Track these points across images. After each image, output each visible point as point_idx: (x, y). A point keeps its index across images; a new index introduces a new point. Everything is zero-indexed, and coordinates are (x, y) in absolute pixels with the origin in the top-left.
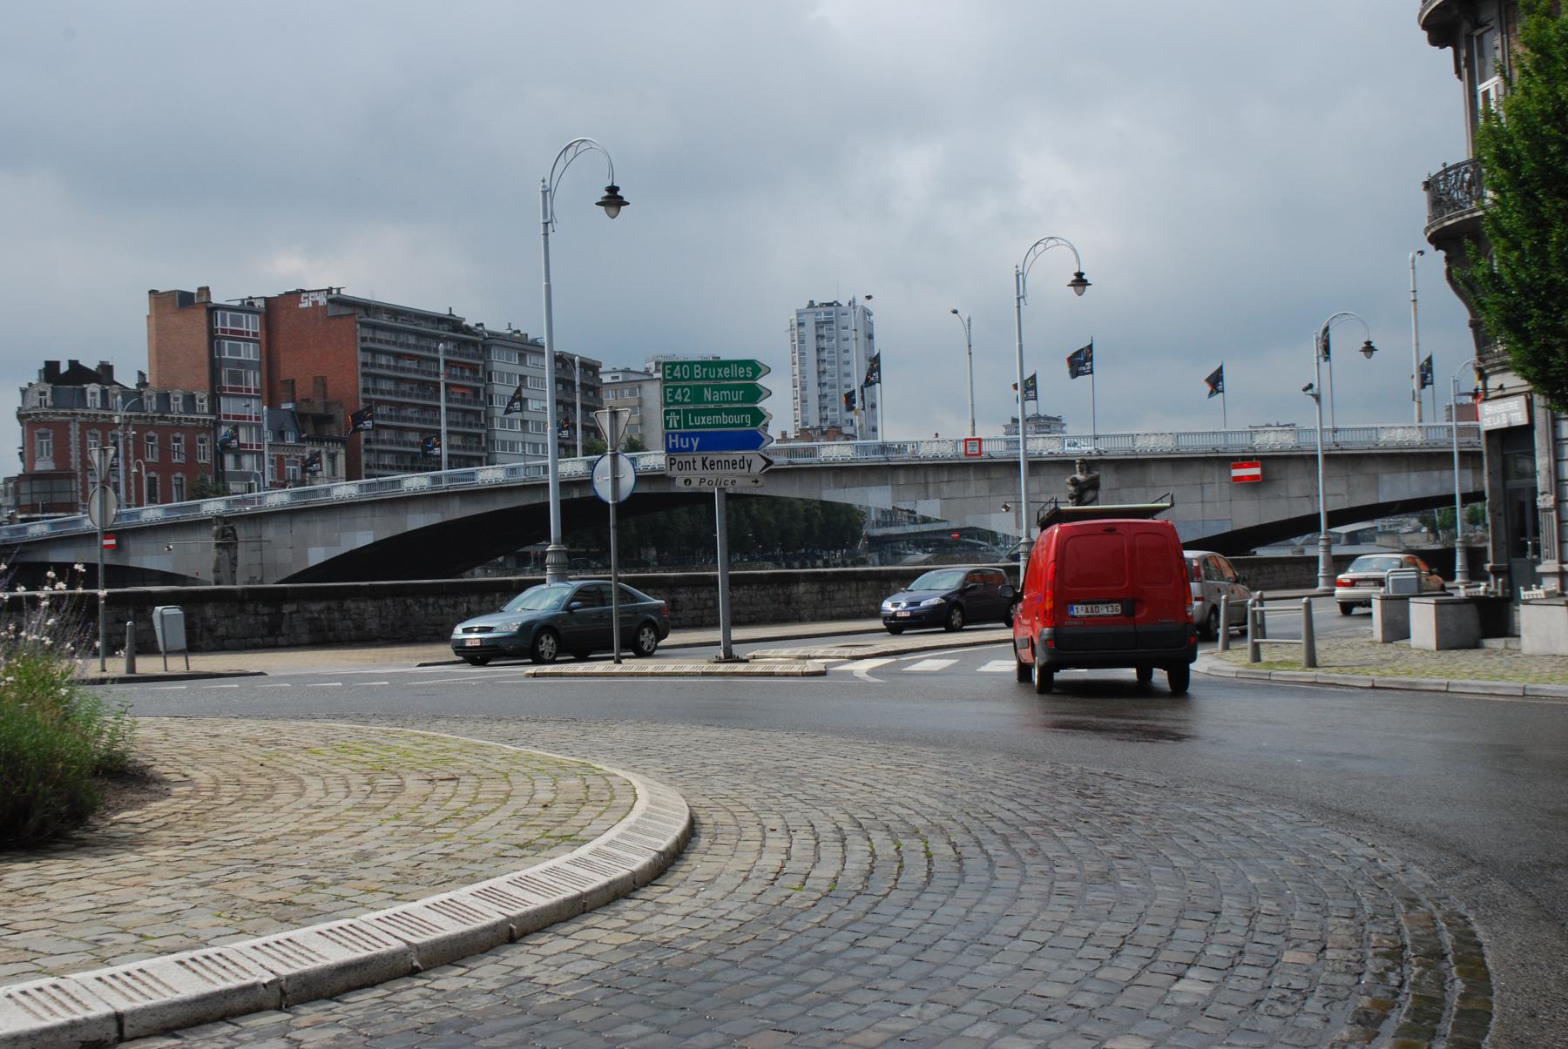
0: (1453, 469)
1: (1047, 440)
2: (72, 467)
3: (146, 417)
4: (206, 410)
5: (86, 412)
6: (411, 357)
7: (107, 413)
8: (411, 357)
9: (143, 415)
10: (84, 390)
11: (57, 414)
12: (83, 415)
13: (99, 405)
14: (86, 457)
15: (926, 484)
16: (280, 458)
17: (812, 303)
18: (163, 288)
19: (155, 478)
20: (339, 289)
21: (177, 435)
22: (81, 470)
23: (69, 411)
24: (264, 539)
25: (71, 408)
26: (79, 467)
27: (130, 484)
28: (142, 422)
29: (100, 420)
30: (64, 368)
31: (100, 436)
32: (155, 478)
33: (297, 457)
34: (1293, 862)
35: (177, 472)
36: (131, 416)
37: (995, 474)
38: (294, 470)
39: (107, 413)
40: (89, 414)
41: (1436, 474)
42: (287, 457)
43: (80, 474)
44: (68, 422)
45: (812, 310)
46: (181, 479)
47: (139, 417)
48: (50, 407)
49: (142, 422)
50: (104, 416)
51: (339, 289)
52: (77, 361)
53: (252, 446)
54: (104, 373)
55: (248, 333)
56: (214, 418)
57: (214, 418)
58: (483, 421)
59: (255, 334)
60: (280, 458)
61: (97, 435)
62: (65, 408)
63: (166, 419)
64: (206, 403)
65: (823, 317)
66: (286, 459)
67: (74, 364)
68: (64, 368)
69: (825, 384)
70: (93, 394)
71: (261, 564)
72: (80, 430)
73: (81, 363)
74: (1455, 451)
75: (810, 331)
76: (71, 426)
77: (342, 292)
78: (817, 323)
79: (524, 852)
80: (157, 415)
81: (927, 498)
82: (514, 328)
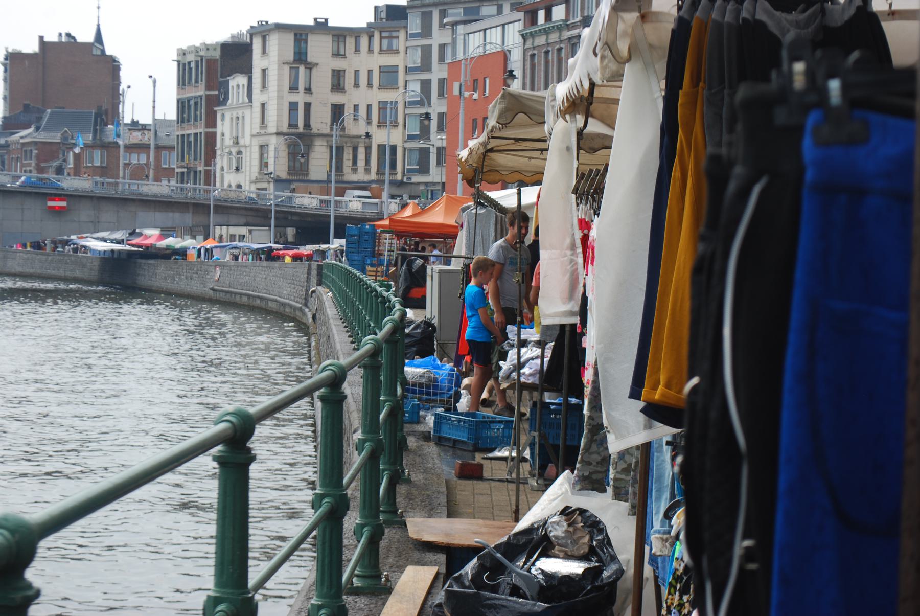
41: (171, 214)
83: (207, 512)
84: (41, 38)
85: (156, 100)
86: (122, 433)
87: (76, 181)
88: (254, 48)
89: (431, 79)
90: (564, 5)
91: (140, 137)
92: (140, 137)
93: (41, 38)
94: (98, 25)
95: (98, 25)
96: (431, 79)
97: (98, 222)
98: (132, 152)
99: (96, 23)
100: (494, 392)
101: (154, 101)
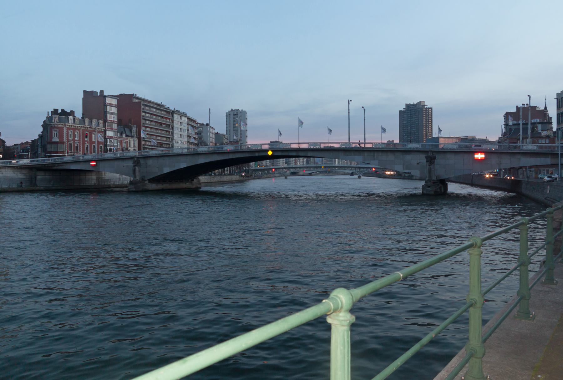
0: (558, 158)
1: (532, 146)
2: (64, 141)
3: (86, 127)
4: (102, 126)
5: (69, 124)
6: (155, 115)
7: (75, 125)
8: (155, 115)
9: (85, 126)
10: (68, 118)
11: (60, 125)
12: (68, 125)
13: (72, 123)
14: (68, 138)
15: (374, 156)
16: (121, 141)
17: (232, 110)
18: (88, 90)
19: (72, 144)
20: (136, 94)
21: (56, 129)
22: (67, 142)
23: (64, 124)
24: (148, 164)
25: (65, 123)
26: (66, 141)
27: (81, 147)
28: (84, 129)
29: (73, 127)
30: (60, 111)
31: (72, 132)
32: (102, 146)
33: (126, 141)
34: (167, 245)
35: (100, 144)
36: (81, 127)
37: (397, 154)
38: (125, 145)
39: (75, 125)
40: (70, 125)
41: (539, 159)
42: (123, 141)
43: (66, 143)
44: (63, 127)
45: (232, 111)
46: (78, 144)
47: (83, 127)
48: (58, 122)
49: (84, 129)
50: (74, 126)
51: (136, 94)
52: (64, 109)
53: (114, 137)
54: (72, 113)
55: (114, 105)
56: (104, 128)
57: (104, 128)
58: (171, 134)
59: (116, 105)
60: (121, 141)
61: (71, 132)
62: (62, 123)
63: (91, 128)
64: (102, 124)
65: (235, 113)
66: (123, 142)
67: (63, 110)
68: (60, 111)
69: (235, 130)
70: (71, 119)
71: (147, 172)
72: (67, 129)
73: (65, 110)
74: (559, 153)
75: (232, 116)
76: (64, 128)
77: (137, 95)
78: (234, 114)
79: (228, 268)
80: (89, 127)
81: (374, 160)
82: (176, 109)
83: (53, 289)
84: (517, 106)
85: (364, 120)
86: (39, 245)
87: (413, 144)
88: (509, 112)
89: (61, 109)
90: (107, 98)
91: (546, 133)
92: (546, 133)
93: (517, 106)
94: (546, 105)
95: (546, 105)
96: (61, 109)
97: (501, 164)
98: (543, 139)
99: (545, 104)
100: (544, 211)
101: (210, 117)
